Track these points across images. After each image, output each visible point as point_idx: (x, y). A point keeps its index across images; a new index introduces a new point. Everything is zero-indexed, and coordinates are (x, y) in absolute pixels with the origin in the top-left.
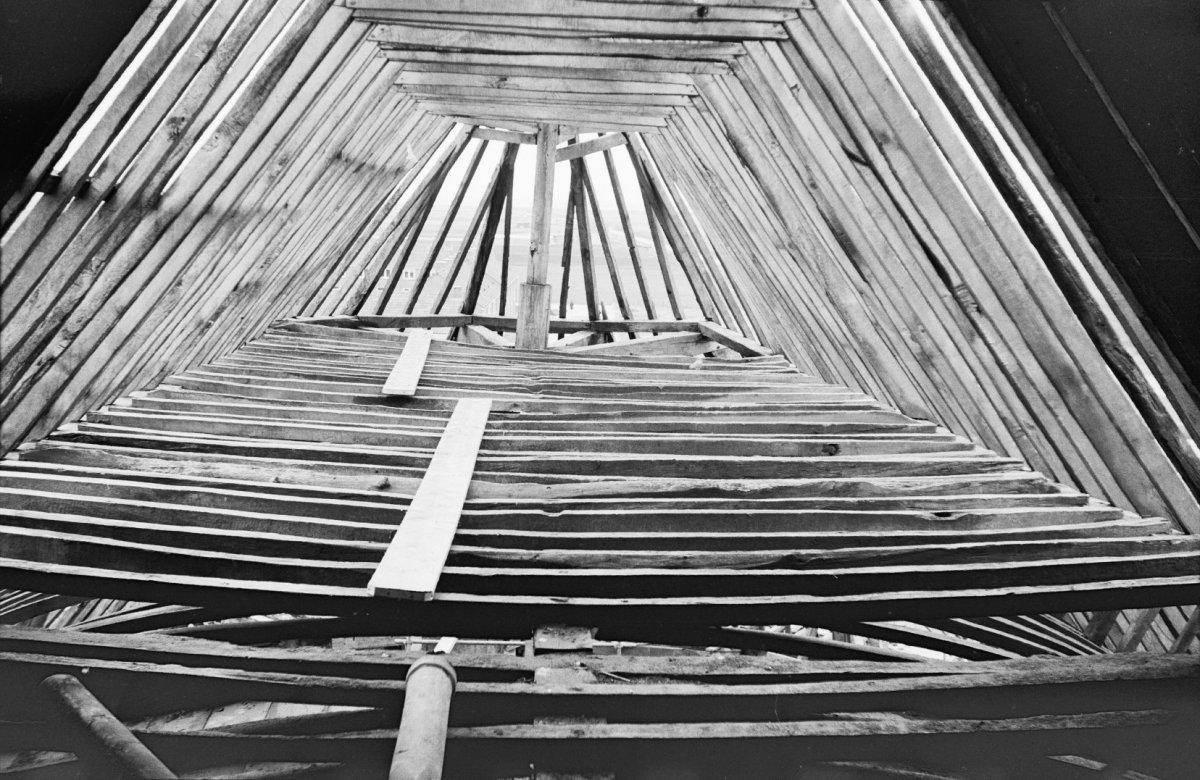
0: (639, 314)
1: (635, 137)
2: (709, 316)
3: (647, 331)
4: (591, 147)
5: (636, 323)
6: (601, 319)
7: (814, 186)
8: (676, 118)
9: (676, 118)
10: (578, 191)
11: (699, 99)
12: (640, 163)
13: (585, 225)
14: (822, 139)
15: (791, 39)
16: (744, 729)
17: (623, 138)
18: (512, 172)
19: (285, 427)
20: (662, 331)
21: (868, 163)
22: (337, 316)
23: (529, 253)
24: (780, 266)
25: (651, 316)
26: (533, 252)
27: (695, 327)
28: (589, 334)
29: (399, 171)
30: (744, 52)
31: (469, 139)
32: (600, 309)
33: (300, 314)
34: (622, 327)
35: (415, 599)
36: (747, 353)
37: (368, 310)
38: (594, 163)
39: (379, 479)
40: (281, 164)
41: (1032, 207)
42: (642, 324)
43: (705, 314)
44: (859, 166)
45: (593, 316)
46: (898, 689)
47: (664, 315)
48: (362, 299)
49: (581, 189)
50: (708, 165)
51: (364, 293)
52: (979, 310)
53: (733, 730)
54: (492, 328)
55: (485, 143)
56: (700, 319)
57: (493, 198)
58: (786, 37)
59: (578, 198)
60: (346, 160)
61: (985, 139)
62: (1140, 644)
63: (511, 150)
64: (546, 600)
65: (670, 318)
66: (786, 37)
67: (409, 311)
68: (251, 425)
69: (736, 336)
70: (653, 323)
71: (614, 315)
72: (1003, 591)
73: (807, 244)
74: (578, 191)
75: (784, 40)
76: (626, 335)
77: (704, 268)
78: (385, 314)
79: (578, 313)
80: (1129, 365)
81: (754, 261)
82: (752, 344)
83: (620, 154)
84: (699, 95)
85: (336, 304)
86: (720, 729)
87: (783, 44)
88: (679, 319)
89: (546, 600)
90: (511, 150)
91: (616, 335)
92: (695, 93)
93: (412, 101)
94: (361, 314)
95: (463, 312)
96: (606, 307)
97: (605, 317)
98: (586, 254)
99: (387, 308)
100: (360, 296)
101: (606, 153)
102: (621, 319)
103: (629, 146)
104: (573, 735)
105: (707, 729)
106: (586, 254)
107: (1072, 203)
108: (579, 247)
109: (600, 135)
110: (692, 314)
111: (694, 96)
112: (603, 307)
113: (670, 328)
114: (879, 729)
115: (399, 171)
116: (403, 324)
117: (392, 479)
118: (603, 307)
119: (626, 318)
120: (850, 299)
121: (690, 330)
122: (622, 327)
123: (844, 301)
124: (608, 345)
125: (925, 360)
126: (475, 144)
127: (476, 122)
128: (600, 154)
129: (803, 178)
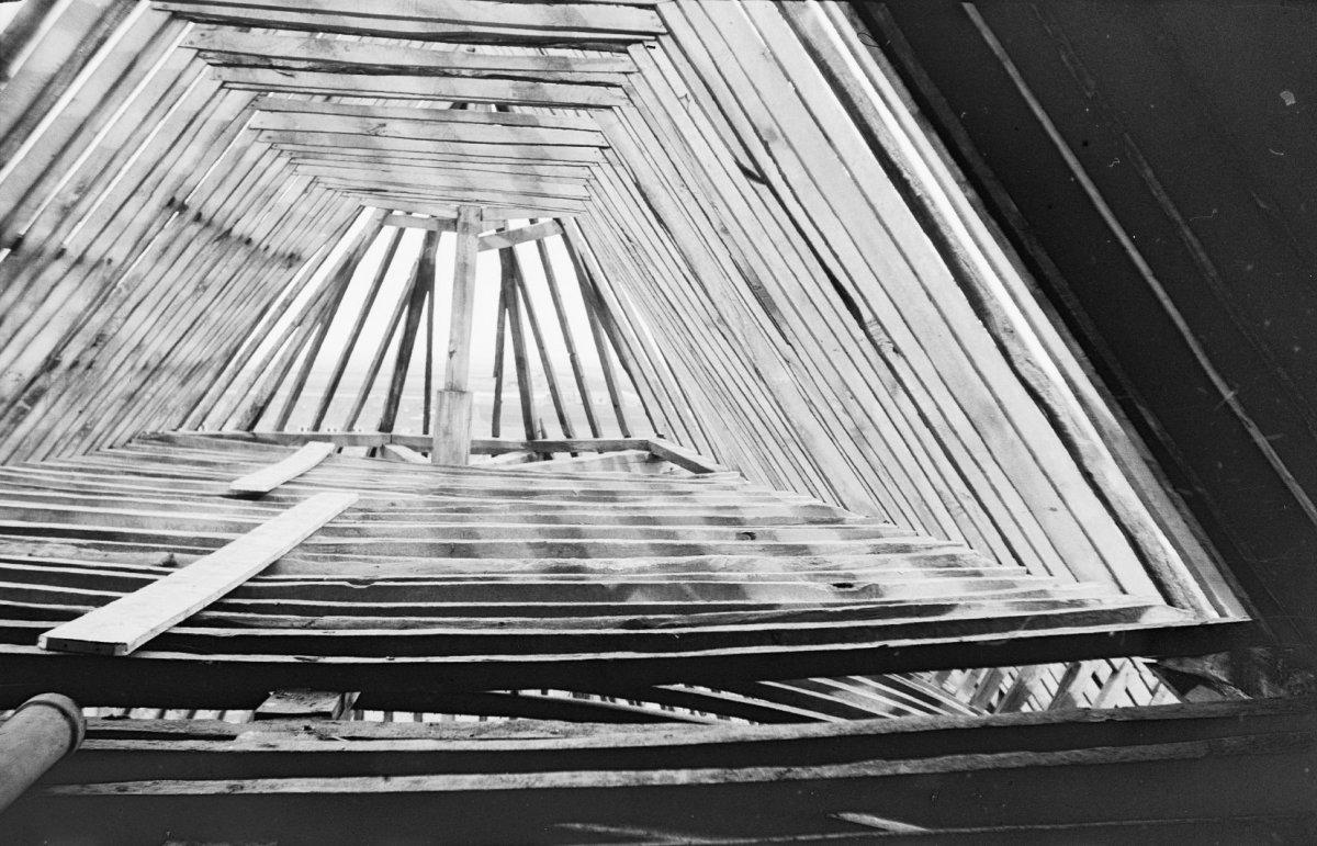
0: (582, 432)
1: (570, 226)
2: (660, 433)
3: (591, 451)
4: (520, 236)
5: (579, 442)
6: (540, 439)
7: (725, 230)
8: (593, 182)
9: (593, 182)
10: (510, 289)
11: (610, 150)
12: (579, 258)
13: (519, 329)
14: (789, 239)
15: (670, 32)
16: (468, 782)
17: (557, 226)
18: (433, 267)
19: (79, 512)
20: (607, 450)
21: (764, 180)
22: (229, 429)
23: (447, 353)
24: (714, 349)
25: (596, 435)
26: (451, 354)
27: (645, 445)
28: (525, 455)
29: (293, 259)
30: (635, 70)
31: (381, 227)
32: (538, 427)
33: (180, 425)
34: (562, 447)
35: (102, 652)
36: (699, 470)
37: (265, 427)
38: (526, 254)
39: (164, 556)
40: (76, 192)
41: (920, 184)
42: (586, 442)
43: (656, 431)
44: (755, 184)
45: (531, 435)
46: (702, 742)
47: (611, 433)
48: (258, 412)
49: (513, 287)
50: (631, 235)
51: (260, 405)
52: (896, 350)
53: (454, 782)
54: (415, 449)
55: (401, 231)
56: (652, 438)
57: (413, 296)
58: (664, 30)
59: (510, 299)
60: (198, 217)
61: (861, 101)
62: (1026, 704)
63: (431, 239)
64: (290, 659)
65: (619, 437)
66: (664, 30)
67: (317, 427)
68: (36, 510)
69: (687, 453)
70: (599, 442)
71: (555, 434)
72: (876, 645)
73: (730, 311)
74: (510, 289)
75: (662, 34)
76: (569, 454)
77: (652, 377)
78: (287, 430)
79: (514, 432)
80: (1044, 381)
81: (691, 352)
82: (705, 461)
83: (554, 243)
84: (610, 147)
85: (226, 413)
86: (435, 782)
87: (661, 37)
88: (627, 436)
89: (290, 659)
90: (431, 239)
91: (556, 455)
92: (606, 144)
93: (283, 160)
94: (258, 429)
95: (380, 430)
96: (544, 425)
97: (544, 437)
98: (521, 362)
99: (291, 421)
100: (256, 409)
101: (540, 244)
102: (561, 437)
103: (565, 236)
104: (227, 791)
105: (418, 782)
106: (521, 362)
107: (942, 147)
108: (513, 360)
109: (532, 221)
110: (642, 432)
111: (606, 148)
112: (542, 426)
113: (617, 447)
114: (652, 779)
115: (293, 259)
116: (304, 440)
117: (177, 556)
118: (542, 426)
119: (568, 436)
120: (780, 377)
121: (639, 448)
122: (562, 447)
123: (775, 379)
124: (547, 462)
125: (858, 438)
126: (389, 232)
127: (389, 204)
128: (533, 244)
129: (714, 223)
